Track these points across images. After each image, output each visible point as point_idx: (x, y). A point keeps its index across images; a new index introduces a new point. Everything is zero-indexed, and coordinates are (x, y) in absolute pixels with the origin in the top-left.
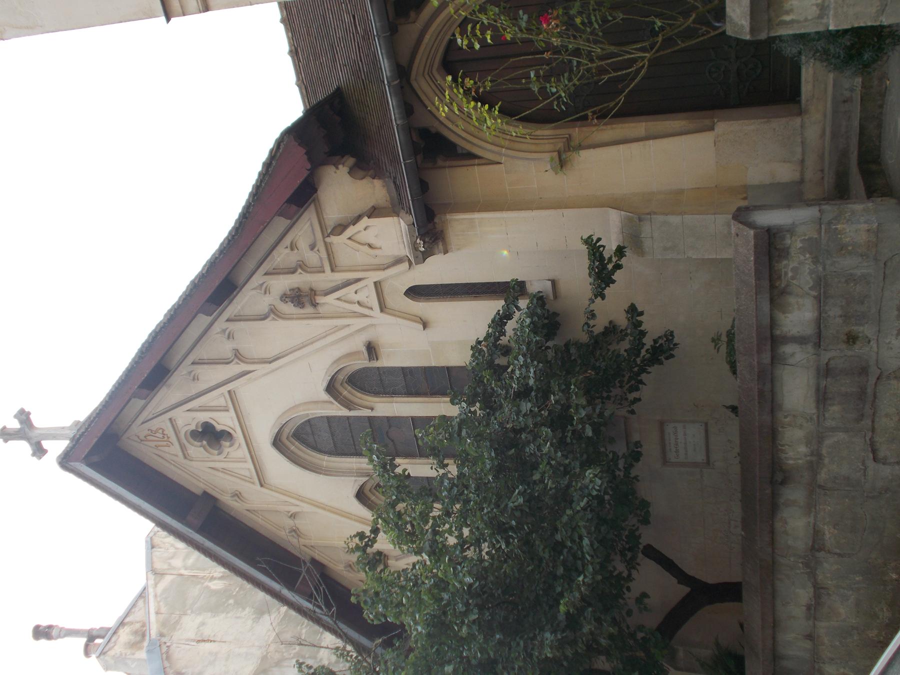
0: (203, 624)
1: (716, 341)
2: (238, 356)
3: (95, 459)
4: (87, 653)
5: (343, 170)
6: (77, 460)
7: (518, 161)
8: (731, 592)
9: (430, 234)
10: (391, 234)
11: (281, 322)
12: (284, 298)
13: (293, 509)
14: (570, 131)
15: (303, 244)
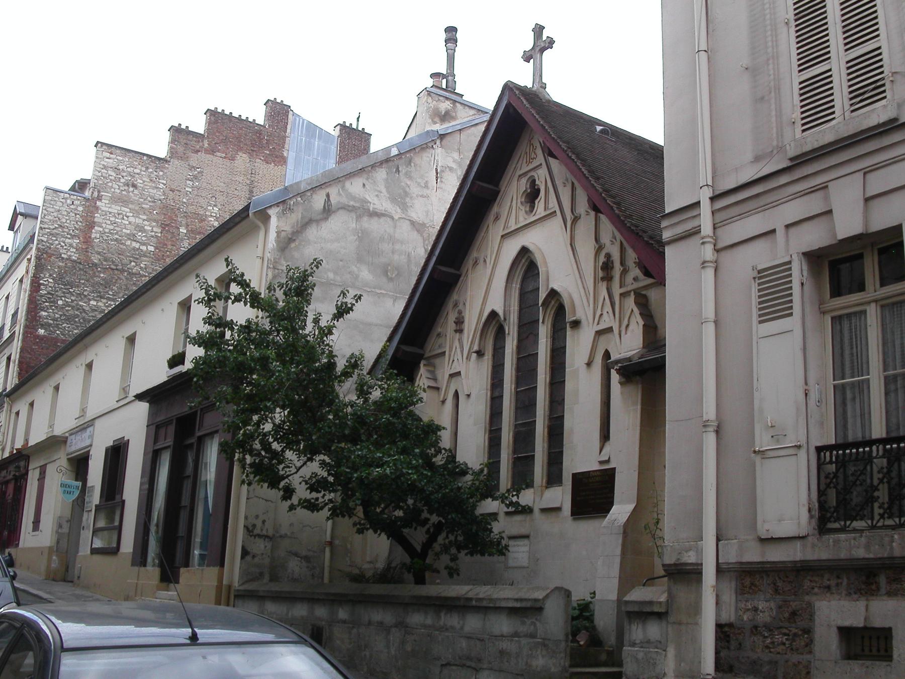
0: (451, 169)
2: (576, 219)
4: (433, 76)
6: (509, 97)
11: (593, 253)
13: (488, 261)
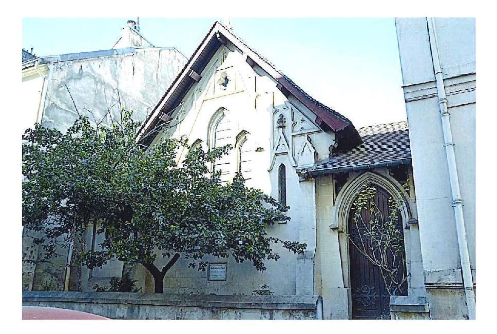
1: (265, 286)
3: (218, 35)
5: (333, 143)
7: (333, 212)
8: (159, 289)
9: (307, 176)
10: (307, 161)
12: (282, 116)
14: (345, 232)
15: (303, 125)
